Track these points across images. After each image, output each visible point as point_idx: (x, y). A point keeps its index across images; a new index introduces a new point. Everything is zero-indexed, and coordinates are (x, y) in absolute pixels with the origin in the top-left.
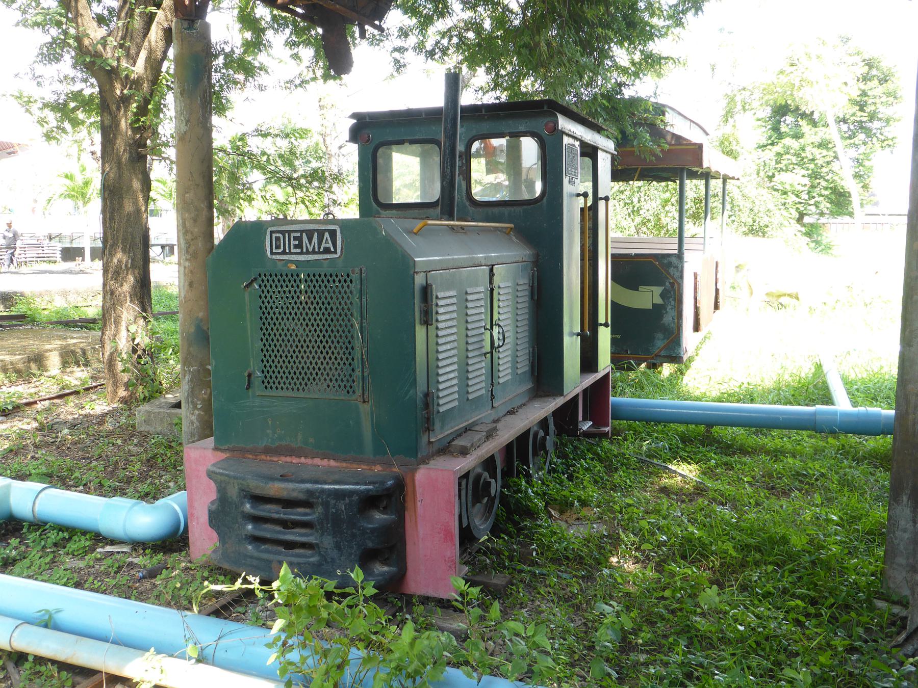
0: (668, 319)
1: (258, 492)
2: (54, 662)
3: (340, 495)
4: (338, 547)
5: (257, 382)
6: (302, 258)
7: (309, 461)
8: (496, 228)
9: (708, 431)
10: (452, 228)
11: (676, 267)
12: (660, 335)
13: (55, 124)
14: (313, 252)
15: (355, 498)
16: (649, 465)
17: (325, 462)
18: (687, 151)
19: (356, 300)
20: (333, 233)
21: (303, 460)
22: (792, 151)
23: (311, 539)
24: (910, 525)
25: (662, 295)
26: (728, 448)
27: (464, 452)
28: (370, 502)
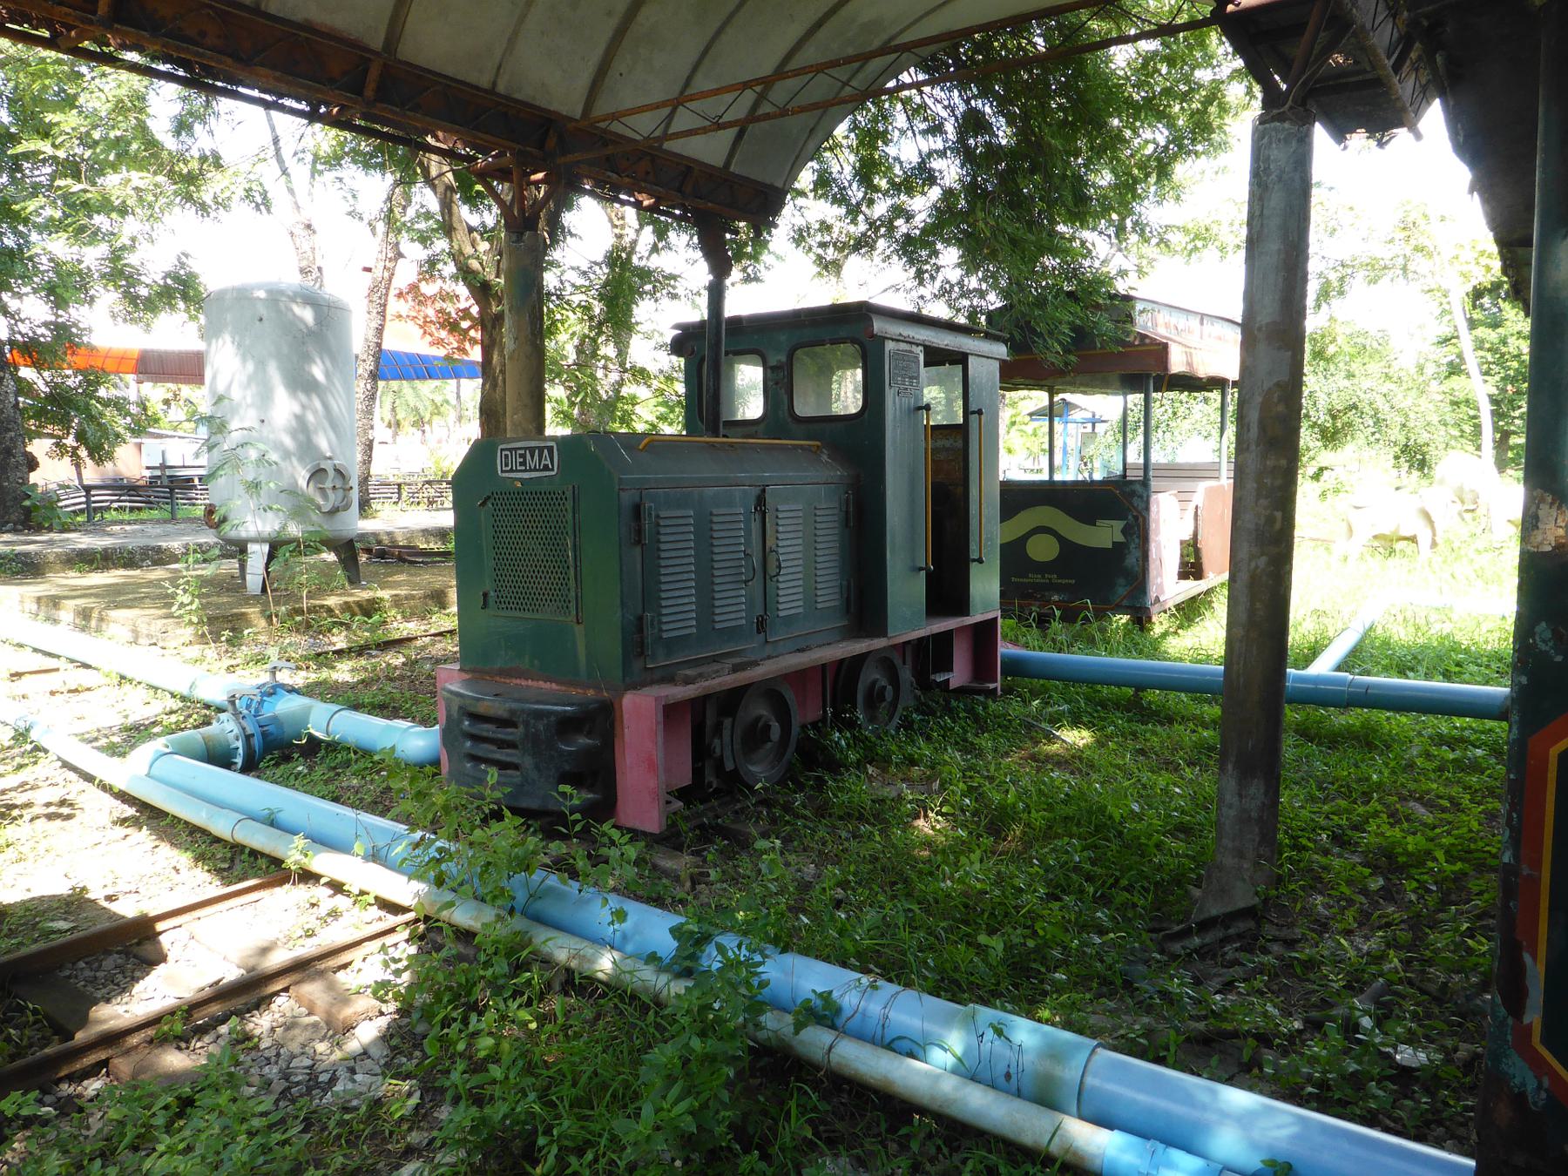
0: (1131, 560)
1: (472, 709)
2: (268, 856)
3: (539, 715)
4: (537, 767)
5: (491, 601)
6: (526, 475)
7: (535, 684)
8: (795, 447)
9: (1136, 694)
10: (712, 445)
11: (1141, 497)
12: (1121, 581)
13: (455, 345)
14: (535, 470)
15: (553, 718)
16: (1033, 731)
17: (547, 685)
18: (1149, 353)
19: (570, 516)
20: (550, 449)
21: (530, 682)
22: (1487, 346)
23: (515, 760)
24: (1235, 800)
25: (1124, 532)
26: (1146, 714)
27: (688, 681)
28: (567, 725)
